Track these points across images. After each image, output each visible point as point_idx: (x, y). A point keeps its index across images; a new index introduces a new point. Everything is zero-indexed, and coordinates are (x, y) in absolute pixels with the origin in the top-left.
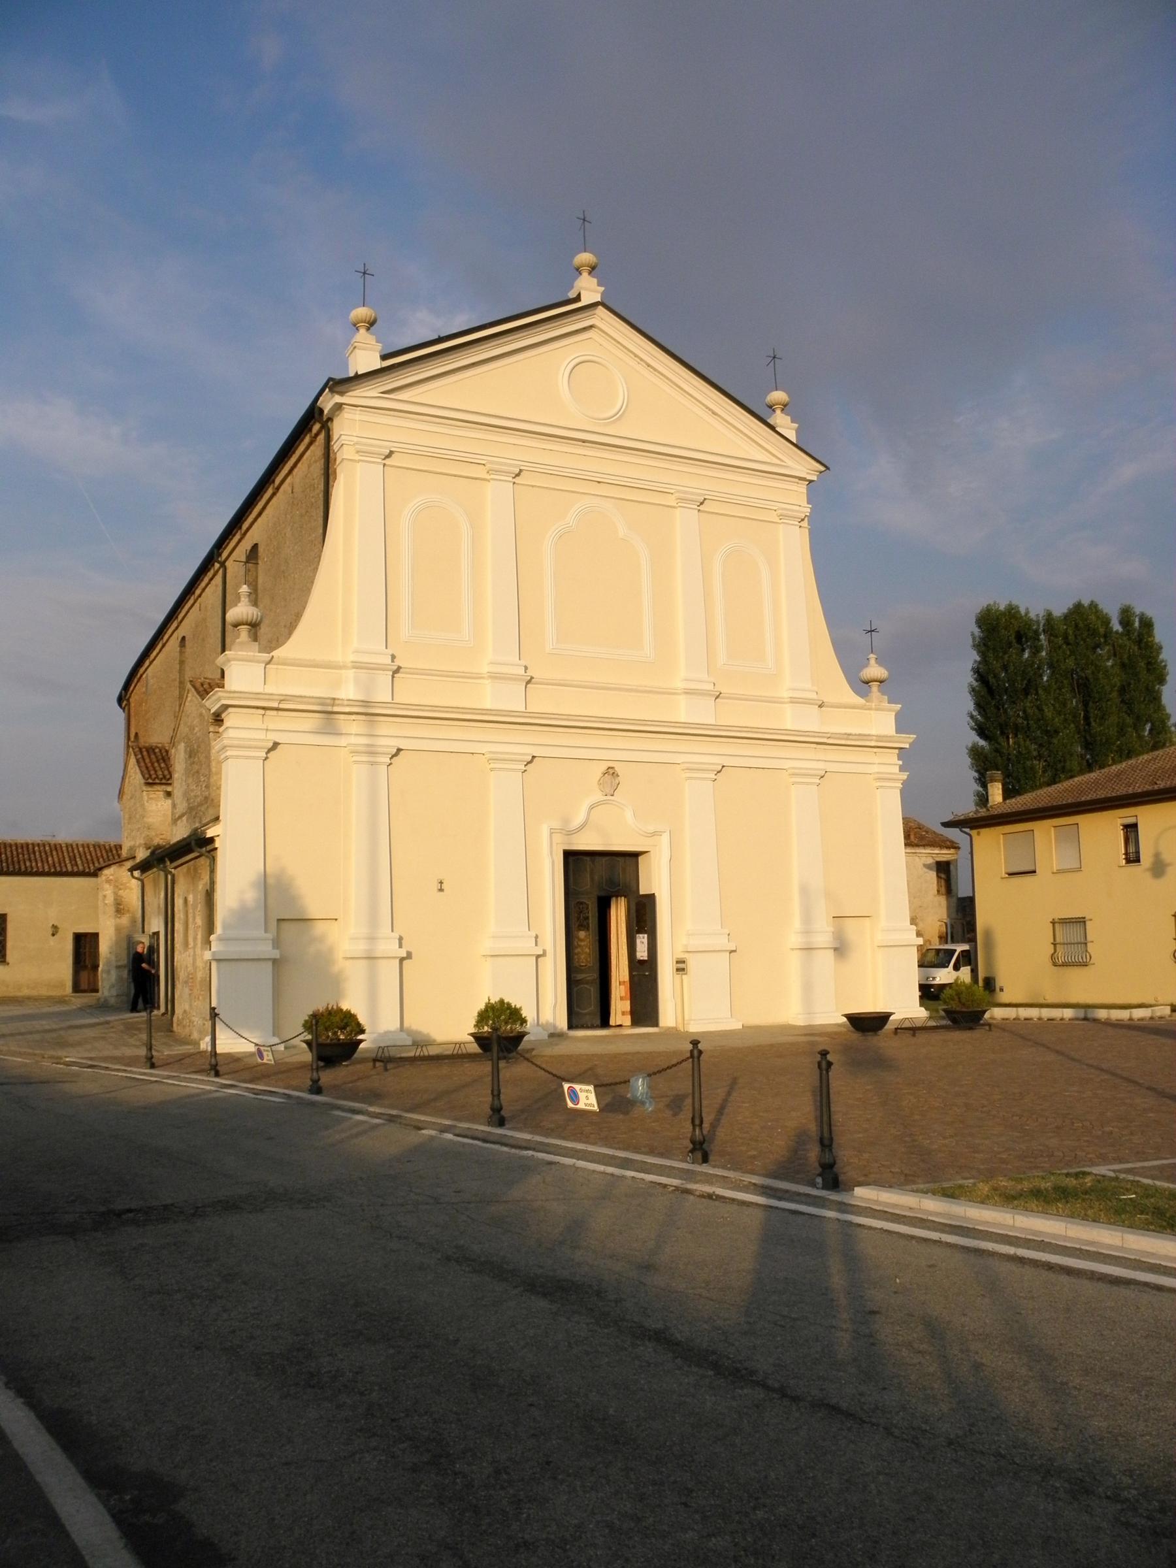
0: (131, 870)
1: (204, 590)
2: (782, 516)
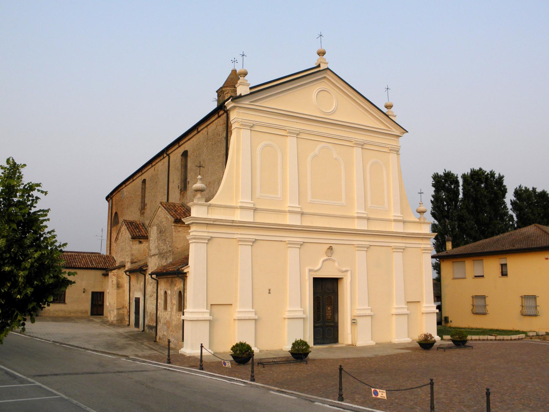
0: (126, 272)
1: (157, 163)
2: (391, 150)
